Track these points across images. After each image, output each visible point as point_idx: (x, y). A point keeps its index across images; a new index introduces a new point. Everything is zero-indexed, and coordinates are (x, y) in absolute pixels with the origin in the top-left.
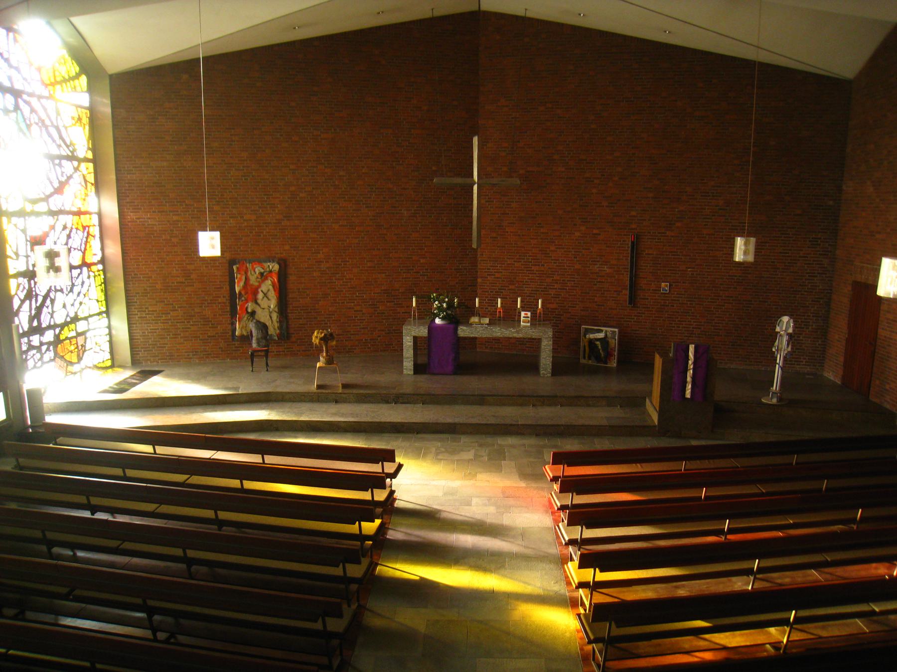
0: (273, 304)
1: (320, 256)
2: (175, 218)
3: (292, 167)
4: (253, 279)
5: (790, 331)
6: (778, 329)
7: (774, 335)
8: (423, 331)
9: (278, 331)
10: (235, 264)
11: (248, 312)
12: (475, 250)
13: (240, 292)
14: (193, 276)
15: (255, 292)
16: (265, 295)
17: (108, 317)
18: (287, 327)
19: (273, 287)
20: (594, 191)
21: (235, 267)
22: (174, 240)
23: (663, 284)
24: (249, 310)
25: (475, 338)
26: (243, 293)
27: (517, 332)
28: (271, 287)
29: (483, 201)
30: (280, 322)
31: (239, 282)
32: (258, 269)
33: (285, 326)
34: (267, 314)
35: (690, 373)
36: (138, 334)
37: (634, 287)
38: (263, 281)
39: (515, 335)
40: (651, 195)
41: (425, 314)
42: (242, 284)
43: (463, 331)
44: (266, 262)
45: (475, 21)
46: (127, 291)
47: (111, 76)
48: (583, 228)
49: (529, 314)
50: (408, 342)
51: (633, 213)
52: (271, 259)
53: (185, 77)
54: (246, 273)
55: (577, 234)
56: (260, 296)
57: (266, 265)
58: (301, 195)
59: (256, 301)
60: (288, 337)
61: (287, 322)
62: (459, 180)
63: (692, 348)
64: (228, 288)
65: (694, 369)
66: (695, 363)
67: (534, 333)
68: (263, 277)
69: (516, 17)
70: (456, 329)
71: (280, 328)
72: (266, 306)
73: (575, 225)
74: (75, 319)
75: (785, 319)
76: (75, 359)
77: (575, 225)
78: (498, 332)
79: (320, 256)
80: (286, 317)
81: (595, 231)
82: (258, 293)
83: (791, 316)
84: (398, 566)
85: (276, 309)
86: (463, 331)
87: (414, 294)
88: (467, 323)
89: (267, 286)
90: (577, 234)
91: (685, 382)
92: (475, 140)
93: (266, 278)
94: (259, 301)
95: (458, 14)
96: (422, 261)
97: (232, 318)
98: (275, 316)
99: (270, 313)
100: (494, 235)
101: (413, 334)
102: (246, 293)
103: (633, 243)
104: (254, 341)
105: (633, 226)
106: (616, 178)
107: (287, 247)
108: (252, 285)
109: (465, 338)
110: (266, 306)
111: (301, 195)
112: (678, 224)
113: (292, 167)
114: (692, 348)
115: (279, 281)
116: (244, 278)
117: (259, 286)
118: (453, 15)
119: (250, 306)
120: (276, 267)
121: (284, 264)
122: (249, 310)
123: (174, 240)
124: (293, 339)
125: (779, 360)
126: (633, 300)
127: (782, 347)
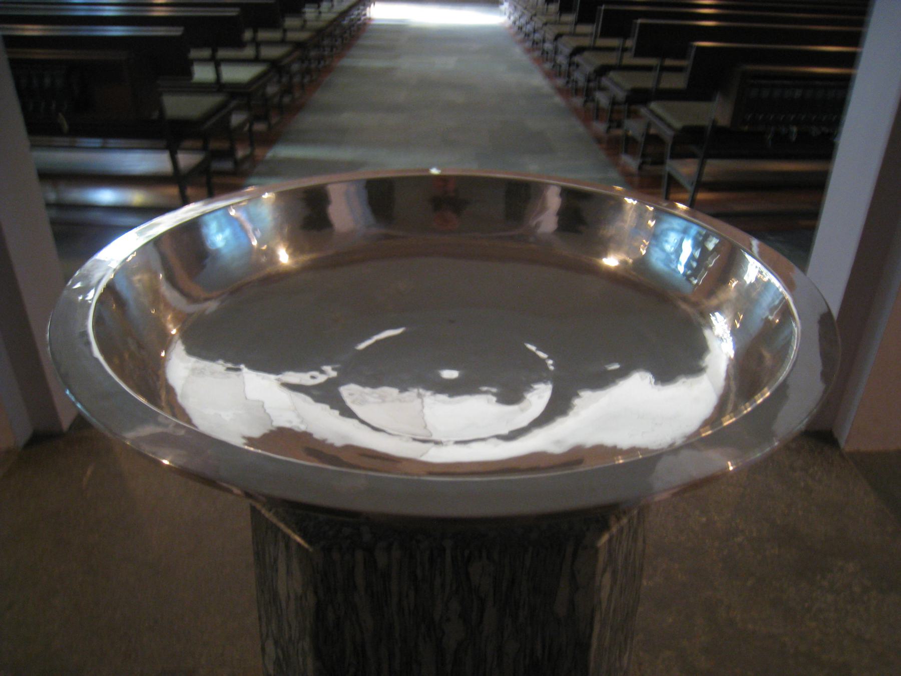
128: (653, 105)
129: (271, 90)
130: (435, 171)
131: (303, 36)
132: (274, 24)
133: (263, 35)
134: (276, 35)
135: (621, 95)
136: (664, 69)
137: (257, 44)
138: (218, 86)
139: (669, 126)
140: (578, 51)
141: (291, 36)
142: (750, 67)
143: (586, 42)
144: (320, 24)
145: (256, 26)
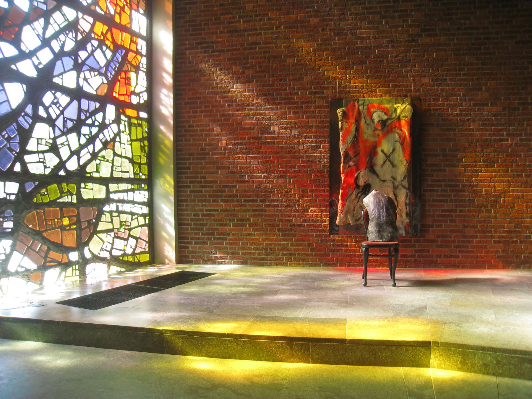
0: (402, 168)
11: (358, 186)
15: (372, 152)
17: (151, 189)
19: (402, 144)
21: (339, 111)
26: (351, 153)
28: (398, 145)
29: (315, 357)
33: (418, 213)
42: (349, 139)
59: (372, 169)
61: (423, 206)
74: (81, 176)
76: (70, 239)
84: (322, 314)
85: (405, 183)
94: (377, 169)
97: (331, 196)
102: (357, 154)
104: (372, 227)
107: (426, 80)
108: (366, 141)
110: (388, 177)
116: (353, 128)
122: (361, 183)
124: (430, 236)
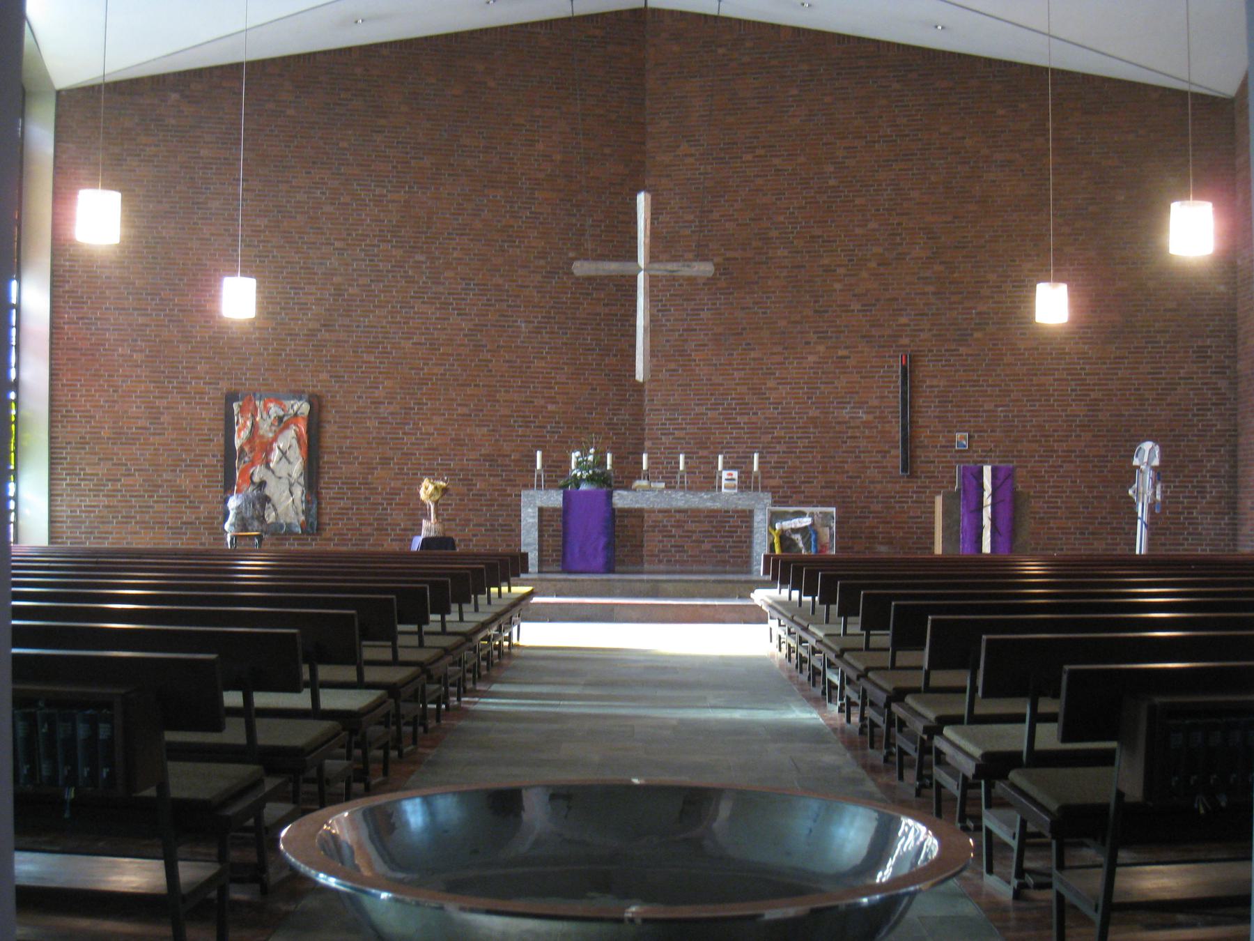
0: (297, 467)
1: (380, 393)
2: (141, 320)
3: (337, 244)
4: (266, 429)
5: (1156, 462)
6: (1136, 462)
7: (1130, 474)
8: (554, 499)
9: (303, 518)
10: (237, 399)
11: (253, 483)
12: (639, 387)
13: (242, 449)
14: (165, 418)
15: (267, 448)
16: (284, 453)
18: (319, 514)
19: (299, 441)
20: (838, 286)
21: (235, 406)
22: (138, 357)
23: (958, 436)
24: (256, 479)
25: (641, 511)
26: (246, 449)
27: (713, 499)
28: (294, 442)
30: (308, 502)
31: (240, 431)
32: (274, 410)
33: (314, 511)
34: (285, 487)
35: (987, 513)
36: (64, 511)
37: (908, 442)
38: (281, 431)
39: (709, 504)
40: (930, 289)
41: (556, 474)
43: (622, 499)
44: (289, 399)
45: (640, 17)
46: (52, 438)
47: (58, 93)
48: (821, 348)
49: (735, 474)
50: (529, 518)
51: (903, 320)
52: (298, 395)
53: (174, 96)
54: (254, 416)
55: (811, 358)
56: (275, 455)
57: (288, 403)
58: (351, 290)
60: (320, 528)
61: (319, 504)
62: (613, 267)
63: (987, 471)
64: (222, 441)
65: (993, 505)
66: (993, 495)
67: (743, 501)
68: (282, 423)
69: (705, 17)
70: (609, 496)
71: (306, 512)
72: (284, 474)
73: (808, 343)
75: (1147, 446)
77: (808, 343)
78: (681, 500)
79: (380, 393)
80: (318, 494)
81: (841, 353)
82: (272, 449)
83: (1155, 441)
85: (302, 480)
86: (622, 499)
87: (537, 448)
88: (627, 487)
89: (288, 439)
90: (811, 358)
91: (981, 528)
92: (642, 199)
93: (287, 427)
95: (611, 13)
96: (551, 407)
97: (226, 492)
98: (298, 491)
99: (291, 485)
100: (672, 366)
101: (539, 503)
103: (904, 368)
105: (905, 341)
106: (873, 264)
107: (324, 376)
108: (262, 437)
109: (622, 510)
111: (351, 290)
112: (977, 335)
113: (337, 244)
114: (987, 471)
115: (308, 431)
116: (249, 424)
117: (275, 439)
118: (603, 15)
119: (258, 473)
120: (305, 408)
121: (317, 405)
122: (256, 479)
123: (138, 357)
125: (1142, 511)
126: (908, 464)
127: (1145, 493)
128: (1014, 775)
129: (335, 766)
130: (636, 781)
131: (396, 675)
132: (349, 657)
133: (324, 672)
134: (349, 673)
135: (969, 768)
136: (1037, 718)
137: (315, 686)
138: (316, 713)
139: (881, 688)
140: (898, 695)
141: (371, 674)
142: (1158, 700)
143: (918, 680)
144: (423, 656)
145: (368, 634)
